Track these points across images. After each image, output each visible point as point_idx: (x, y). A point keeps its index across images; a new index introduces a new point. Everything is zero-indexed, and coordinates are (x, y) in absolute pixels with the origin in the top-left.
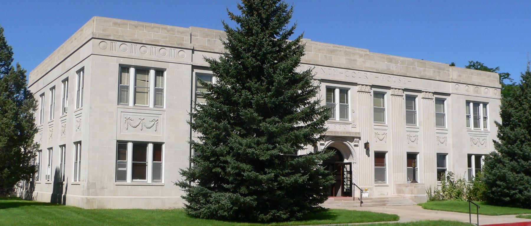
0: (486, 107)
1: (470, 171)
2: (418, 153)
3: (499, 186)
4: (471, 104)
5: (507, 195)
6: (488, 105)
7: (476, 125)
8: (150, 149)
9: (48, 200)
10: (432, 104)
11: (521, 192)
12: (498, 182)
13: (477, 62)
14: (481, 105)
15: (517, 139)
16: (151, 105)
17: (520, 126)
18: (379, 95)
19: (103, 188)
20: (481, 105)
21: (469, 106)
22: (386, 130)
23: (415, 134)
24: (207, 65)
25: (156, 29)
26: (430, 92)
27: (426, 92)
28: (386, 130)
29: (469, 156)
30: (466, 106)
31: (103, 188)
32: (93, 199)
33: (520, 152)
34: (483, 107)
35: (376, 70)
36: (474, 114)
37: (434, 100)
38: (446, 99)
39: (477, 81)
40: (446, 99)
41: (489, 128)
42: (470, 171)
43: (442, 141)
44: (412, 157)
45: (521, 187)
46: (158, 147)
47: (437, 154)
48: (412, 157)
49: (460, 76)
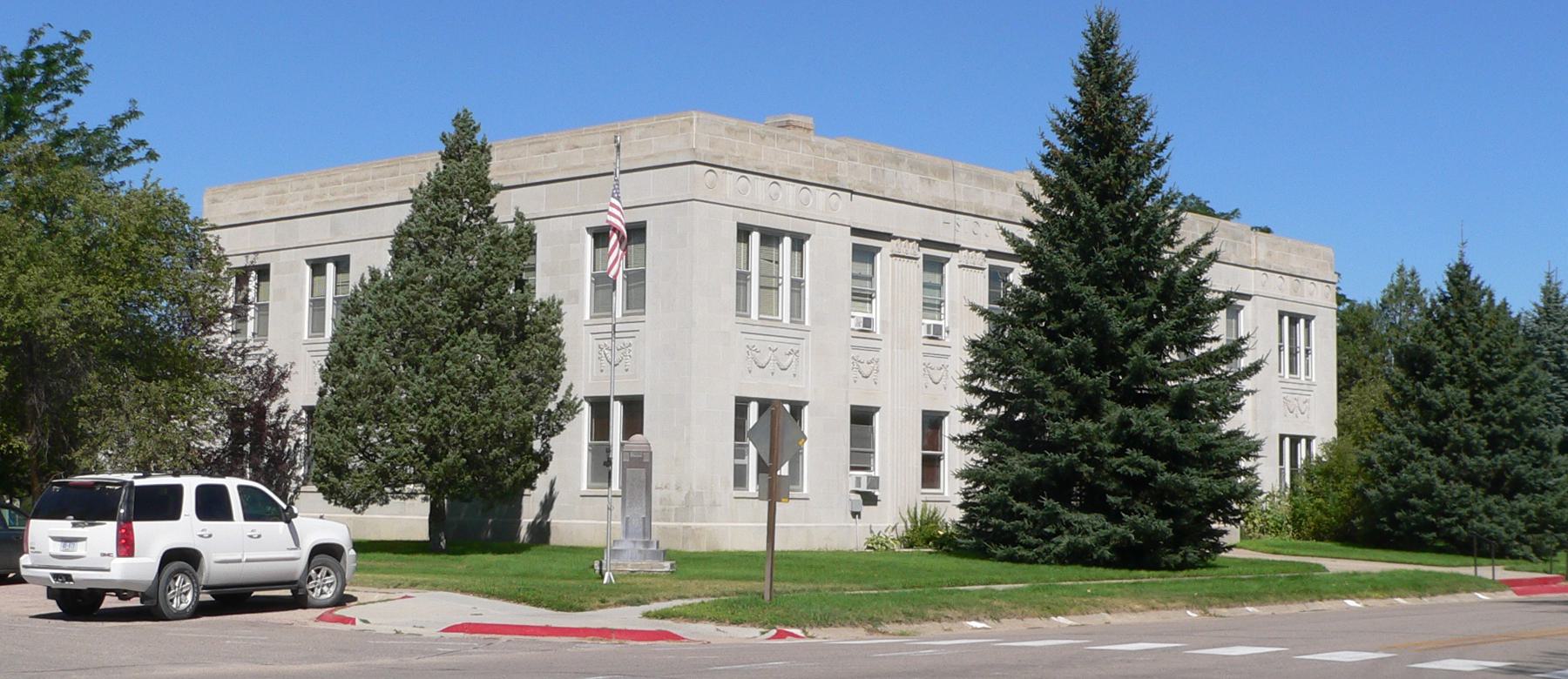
0: (801, 250)
1: (1282, 472)
2: (878, 409)
3: (1414, 508)
4: (755, 237)
5: (1431, 527)
6: (807, 245)
7: (1293, 369)
8: (617, 410)
9: (421, 533)
10: (915, 270)
11: (1462, 521)
12: (1413, 500)
13: (1192, 197)
14: (787, 241)
15: (1450, 410)
16: (786, 320)
17: (1452, 381)
18: (934, 265)
19: (714, 504)
20: (787, 241)
21: (747, 241)
22: (877, 350)
23: (872, 355)
24: (1010, 250)
25: (794, 144)
26: (911, 240)
27: (903, 239)
28: (877, 350)
29: (1282, 437)
30: (739, 240)
31: (714, 504)
32: (701, 529)
33: (1458, 437)
34: (793, 249)
35: (1006, 214)
36: (1290, 342)
37: (921, 261)
38: (879, 249)
39: (1296, 266)
40: (879, 249)
41: (1313, 377)
42: (1282, 472)
43: (866, 369)
44: (862, 417)
45: (1464, 511)
46: (634, 407)
47: (852, 407)
48: (862, 417)
49: (1269, 254)
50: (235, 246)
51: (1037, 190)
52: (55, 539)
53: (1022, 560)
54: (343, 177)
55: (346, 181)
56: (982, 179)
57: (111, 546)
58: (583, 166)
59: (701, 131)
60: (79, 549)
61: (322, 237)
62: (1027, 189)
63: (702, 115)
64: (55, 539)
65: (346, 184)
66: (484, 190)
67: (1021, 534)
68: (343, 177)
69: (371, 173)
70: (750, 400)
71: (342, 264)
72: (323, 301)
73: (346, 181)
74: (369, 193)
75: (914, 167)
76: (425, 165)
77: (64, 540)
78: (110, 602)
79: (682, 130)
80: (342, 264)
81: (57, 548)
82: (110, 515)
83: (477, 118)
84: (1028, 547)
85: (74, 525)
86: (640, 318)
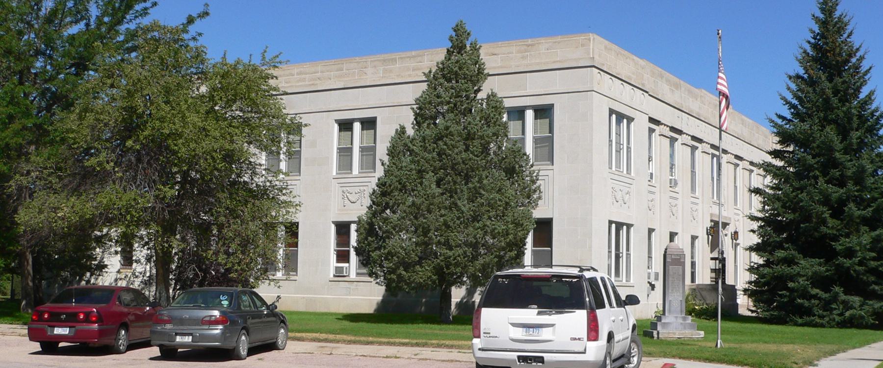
44: (651, 231)
50: (291, 106)
51: (789, 97)
52: (514, 325)
53: (816, 325)
54: (296, 71)
55: (298, 74)
56: (690, 92)
57: (583, 332)
58: (502, 67)
59: (597, 47)
60: (545, 334)
61: (357, 103)
62: (784, 95)
63: (595, 36)
64: (514, 325)
65: (372, 70)
66: (479, 75)
67: (815, 309)
68: (296, 71)
69: (319, 68)
70: (350, 223)
71: (369, 124)
72: (350, 150)
73: (298, 74)
74: (318, 82)
75: (668, 81)
76: (433, 58)
77: (527, 326)
78: (61, 345)
79: (583, 45)
80: (369, 124)
81: (519, 333)
82: (580, 305)
83: (468, 28)
84: (822, 317)
85: (539, 313)
86: (297, 178)
